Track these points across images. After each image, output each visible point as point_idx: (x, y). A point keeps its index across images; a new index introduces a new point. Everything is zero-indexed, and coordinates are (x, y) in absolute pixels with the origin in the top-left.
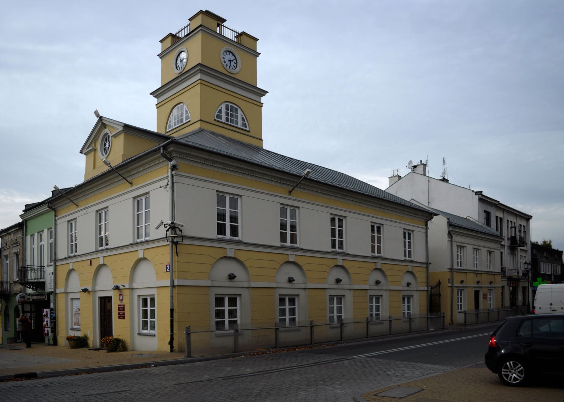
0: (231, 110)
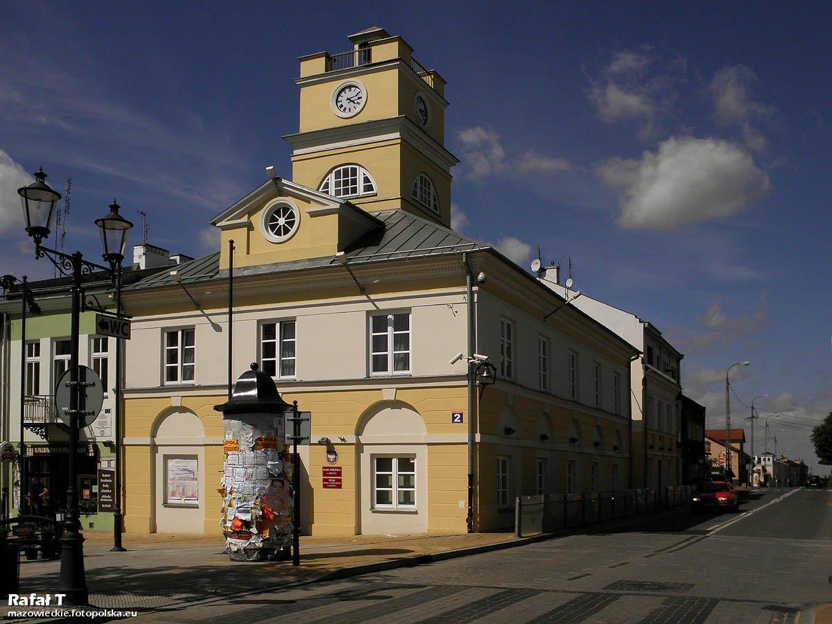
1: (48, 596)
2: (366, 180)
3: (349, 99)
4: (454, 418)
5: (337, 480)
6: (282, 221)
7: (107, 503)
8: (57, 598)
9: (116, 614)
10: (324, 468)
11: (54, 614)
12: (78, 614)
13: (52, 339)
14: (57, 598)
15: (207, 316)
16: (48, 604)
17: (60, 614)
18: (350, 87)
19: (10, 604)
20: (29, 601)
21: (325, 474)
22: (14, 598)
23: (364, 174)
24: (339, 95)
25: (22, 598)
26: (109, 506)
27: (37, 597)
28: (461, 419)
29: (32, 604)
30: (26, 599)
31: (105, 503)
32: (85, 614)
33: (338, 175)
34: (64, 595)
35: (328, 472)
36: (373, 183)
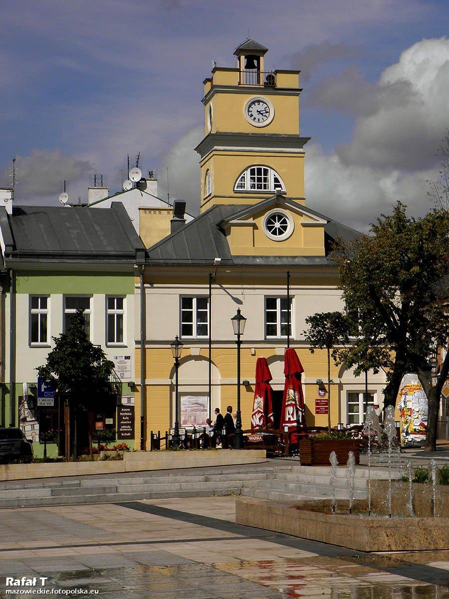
0: (259, 174)
1: (35, 579)
2: (276, 180)
3: (259, 112)
5: (326, 408)
6: (277, 225)
7: (127, 432)
8: (41, 580)
9: (83, 592)
10: (316, 400)
11: (39, 592)
12: (56, 592)
13: (63, 295)
14: (41, 580)
15: (224, 289)
16: (34, 585)
17: (43, 592)
18: (259, 102)
19: (7, 584)
20: (21, 583)
21: (317, 404)
22: (10, 580)
23: (275, 176)
24: (250, 106)
25: (15, 580)
26: (129, 434)
27: (26, 579)
29: (23, 584)
30: (19, 581)
31: (124, 432)
32: (61, 592)
33: (253, 172)
34: (46, 578)
35: (319, 403)
36: (282, 183)
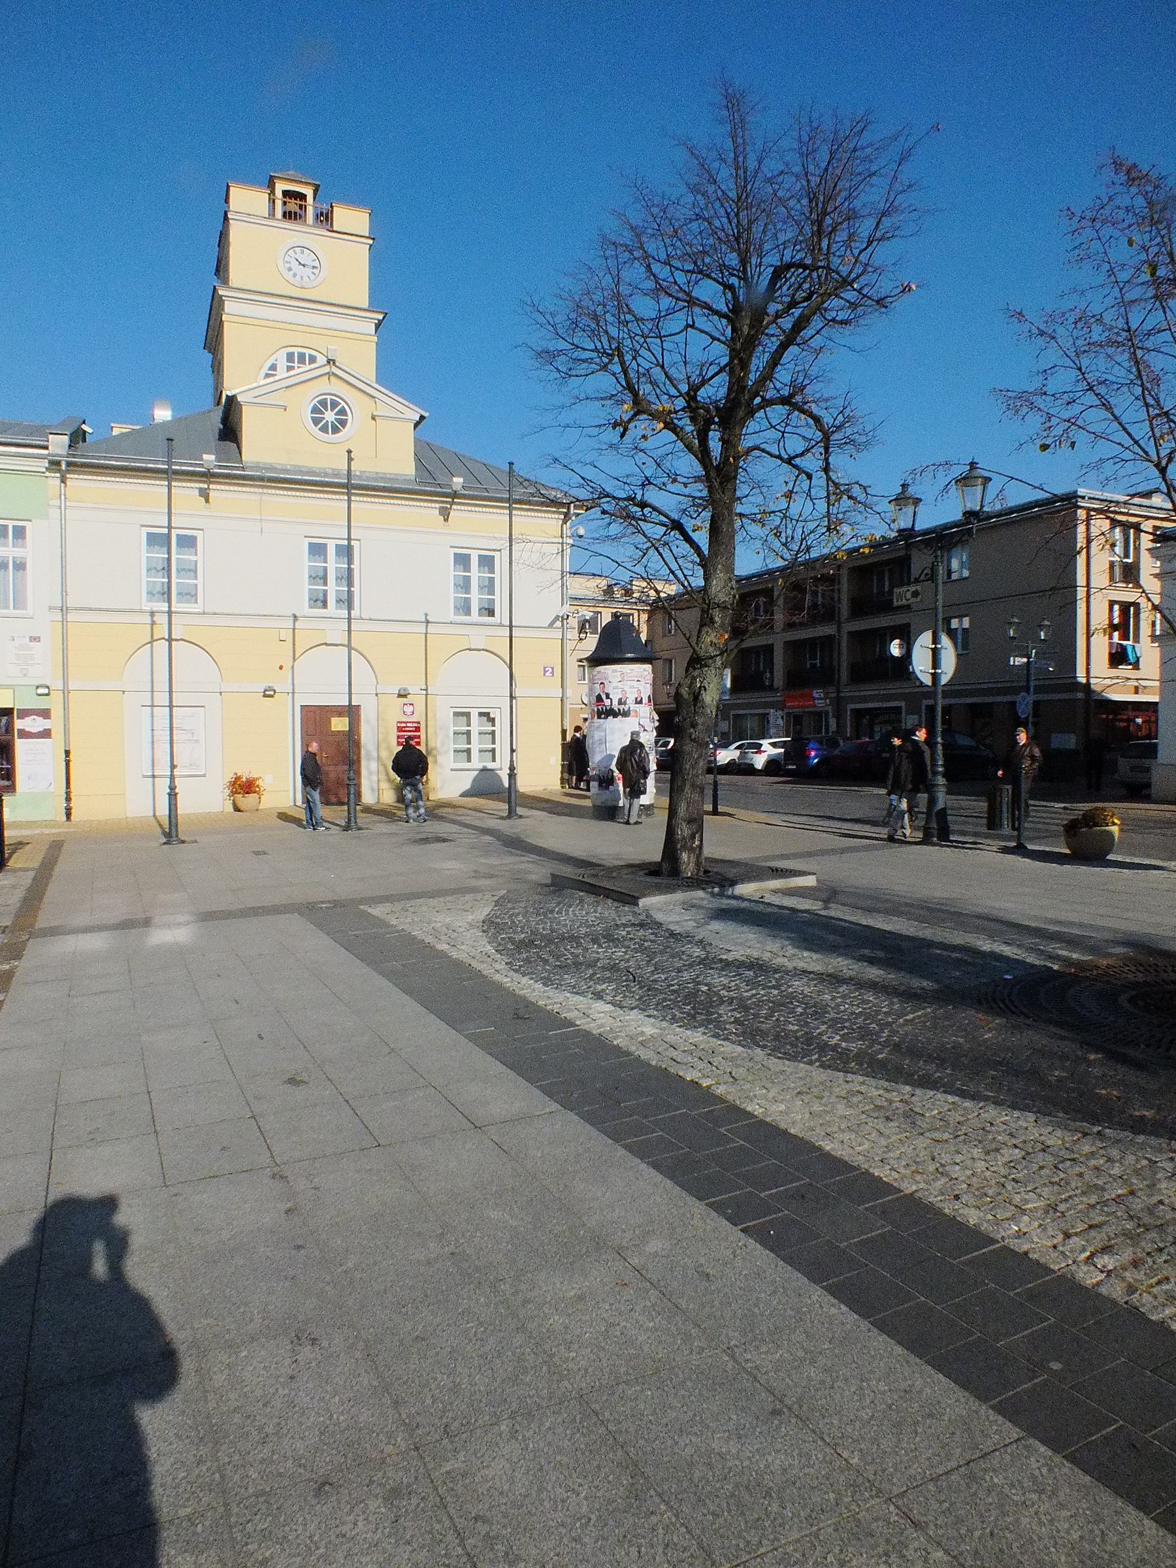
4: (545, 672)
21: (400, 729)
28: (552, 673)
